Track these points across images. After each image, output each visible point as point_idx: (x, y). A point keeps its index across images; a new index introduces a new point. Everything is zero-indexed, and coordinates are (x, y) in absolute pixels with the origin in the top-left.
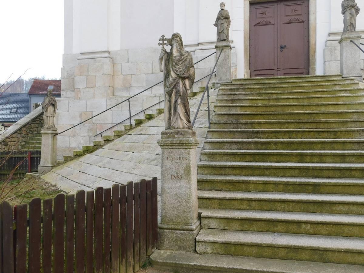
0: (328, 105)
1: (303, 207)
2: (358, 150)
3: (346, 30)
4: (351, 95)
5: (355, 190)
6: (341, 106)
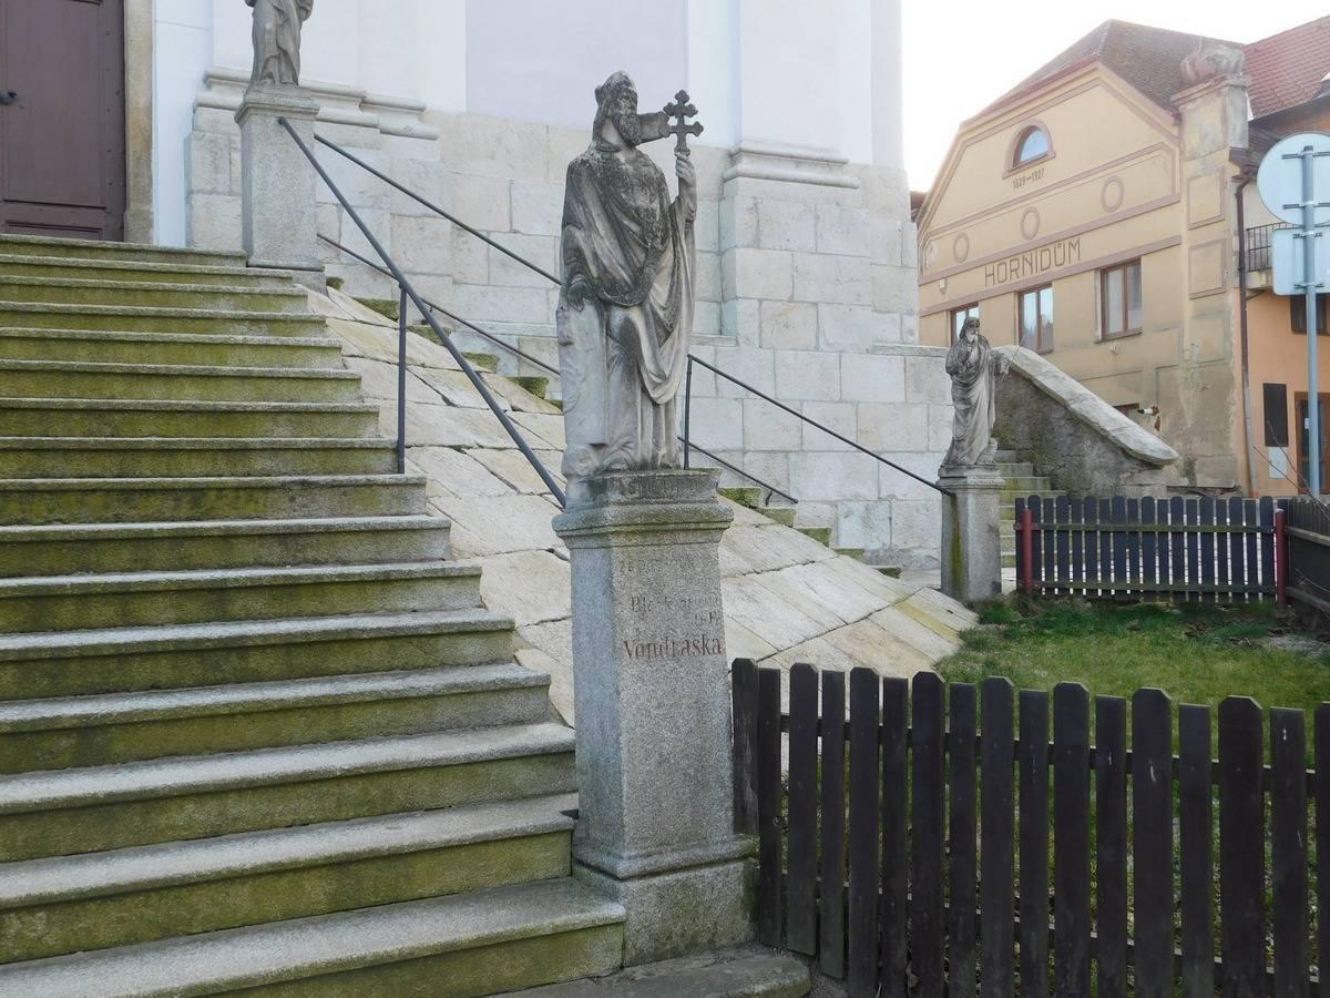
0: (180, 376)
1: (20, 838)
2: (283, 565)
3: (261, 73)
4: (272, 339)
5: (252, 731)
6: (231, 382)
